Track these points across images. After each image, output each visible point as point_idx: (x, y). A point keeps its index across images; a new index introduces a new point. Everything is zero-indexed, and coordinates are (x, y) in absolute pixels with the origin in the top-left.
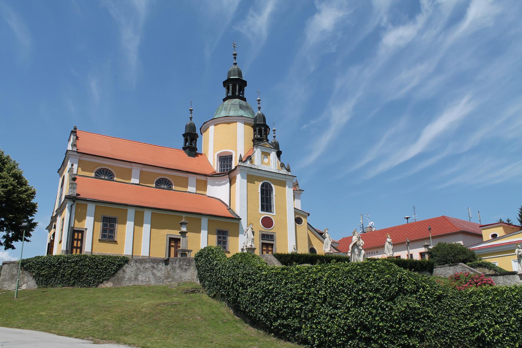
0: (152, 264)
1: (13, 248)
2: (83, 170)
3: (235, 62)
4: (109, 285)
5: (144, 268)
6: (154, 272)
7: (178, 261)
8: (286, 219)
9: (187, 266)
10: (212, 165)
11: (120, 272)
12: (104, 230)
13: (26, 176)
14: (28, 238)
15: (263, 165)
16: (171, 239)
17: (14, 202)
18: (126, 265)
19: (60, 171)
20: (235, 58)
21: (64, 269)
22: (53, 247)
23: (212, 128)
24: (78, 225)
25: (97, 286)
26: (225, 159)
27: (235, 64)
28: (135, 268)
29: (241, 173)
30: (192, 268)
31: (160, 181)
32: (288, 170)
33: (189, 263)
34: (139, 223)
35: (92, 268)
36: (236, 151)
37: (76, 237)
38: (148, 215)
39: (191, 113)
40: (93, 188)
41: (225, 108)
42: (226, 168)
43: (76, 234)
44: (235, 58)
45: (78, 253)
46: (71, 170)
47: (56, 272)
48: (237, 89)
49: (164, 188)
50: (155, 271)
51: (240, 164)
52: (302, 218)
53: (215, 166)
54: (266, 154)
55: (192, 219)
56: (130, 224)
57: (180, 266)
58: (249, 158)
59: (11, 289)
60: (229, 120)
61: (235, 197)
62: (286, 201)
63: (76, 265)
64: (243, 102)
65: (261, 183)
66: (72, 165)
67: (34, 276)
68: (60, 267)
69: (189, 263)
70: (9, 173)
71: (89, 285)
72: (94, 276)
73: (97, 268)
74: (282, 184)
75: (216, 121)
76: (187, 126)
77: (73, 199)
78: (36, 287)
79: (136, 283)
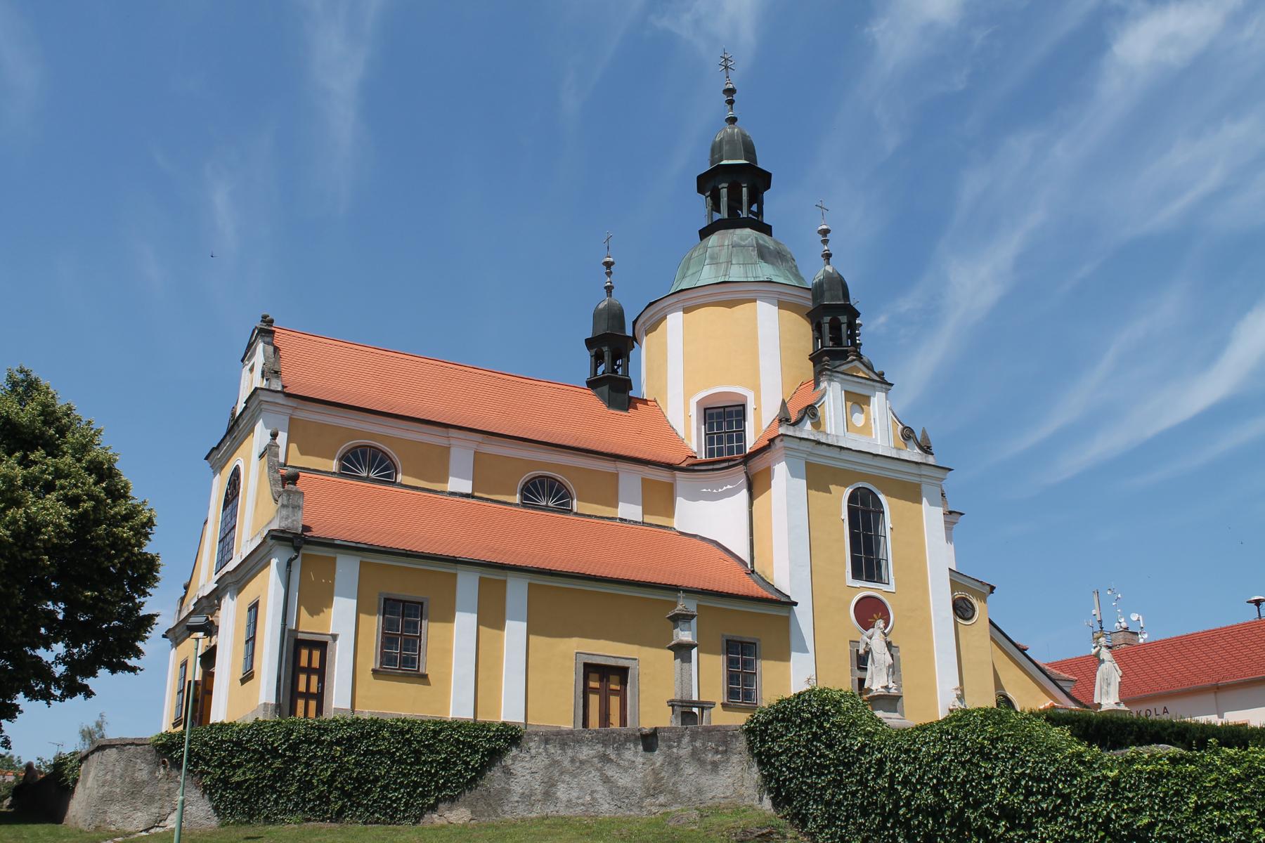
0: (599, 748)
1: (89, 693)
2: (304, 451)
3: (730, 114)
4: (458, 815)
5: (573, 761)
6: (609, 773)
7: (686, 740)
8: (927, 602)
9: (717, 752)
10: (682, 433)
11: (495, 773)
12: (388, 640)
13: (127, 471)
14: (132, 662)
15: (852, 435)
16: (591, 670)
17: (97, 549)
18: (514, 751)
19: (217, 455)
20: (731, 102)
21: (307, 765)
22: (210, 693)
23: (675, 321)
24: (308, 625)
25: (418, 819)
26: (723, 418)
27: (732, 120)
28: (542, 761)
29: (787, 458)
30: (735, 758)
31: (534, 485)
32: (926, 450)
33: (725, 743)
34: (491, 617)
35: (401, 761)
36: (757, 390)
37: (304, 662)
38: (517, 590)
39: (609, 274)
40: (343, 507)
41: (712, 258)
42: (725, 445)
43: (304, 653)
44: (731, 102)
45: (312, 713)
46: (268, 452)
47: (280, 776)
48: (745, 198)
49: (546, 509)
50: (611, 771)
51: (782, 431)
52: (974, 601)
53: (692, 437)
54: (858, 401)
55: (649, 603)
56: (465, 622)
57: (695, 754)
58: (811, 411)
59: (131, 829)
60: (728, 295)
61: (774, 533)
62: (924, 544)
63: (349, 751)
64: (765, 237)
65: (848, 491)
66: (274, 436)
67: (205, 787)
68: (295, 759)
69: (725, 743)
70: (79, 460)
71: (392, 817)
72: (407, 786)
73: (418, 761)
74: (911, 493)
75: (689, 299)
76: (597, 315)
77: (292, 542)
78: (215, 822)
79: (550, 810)
